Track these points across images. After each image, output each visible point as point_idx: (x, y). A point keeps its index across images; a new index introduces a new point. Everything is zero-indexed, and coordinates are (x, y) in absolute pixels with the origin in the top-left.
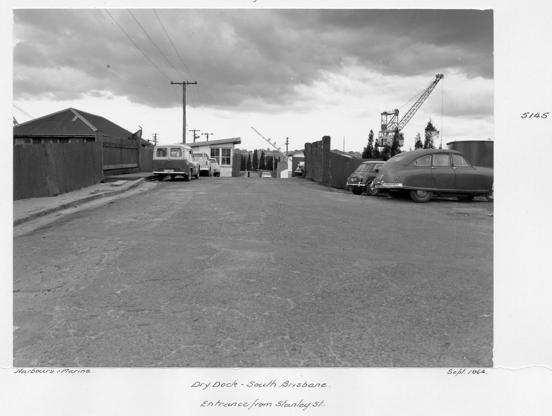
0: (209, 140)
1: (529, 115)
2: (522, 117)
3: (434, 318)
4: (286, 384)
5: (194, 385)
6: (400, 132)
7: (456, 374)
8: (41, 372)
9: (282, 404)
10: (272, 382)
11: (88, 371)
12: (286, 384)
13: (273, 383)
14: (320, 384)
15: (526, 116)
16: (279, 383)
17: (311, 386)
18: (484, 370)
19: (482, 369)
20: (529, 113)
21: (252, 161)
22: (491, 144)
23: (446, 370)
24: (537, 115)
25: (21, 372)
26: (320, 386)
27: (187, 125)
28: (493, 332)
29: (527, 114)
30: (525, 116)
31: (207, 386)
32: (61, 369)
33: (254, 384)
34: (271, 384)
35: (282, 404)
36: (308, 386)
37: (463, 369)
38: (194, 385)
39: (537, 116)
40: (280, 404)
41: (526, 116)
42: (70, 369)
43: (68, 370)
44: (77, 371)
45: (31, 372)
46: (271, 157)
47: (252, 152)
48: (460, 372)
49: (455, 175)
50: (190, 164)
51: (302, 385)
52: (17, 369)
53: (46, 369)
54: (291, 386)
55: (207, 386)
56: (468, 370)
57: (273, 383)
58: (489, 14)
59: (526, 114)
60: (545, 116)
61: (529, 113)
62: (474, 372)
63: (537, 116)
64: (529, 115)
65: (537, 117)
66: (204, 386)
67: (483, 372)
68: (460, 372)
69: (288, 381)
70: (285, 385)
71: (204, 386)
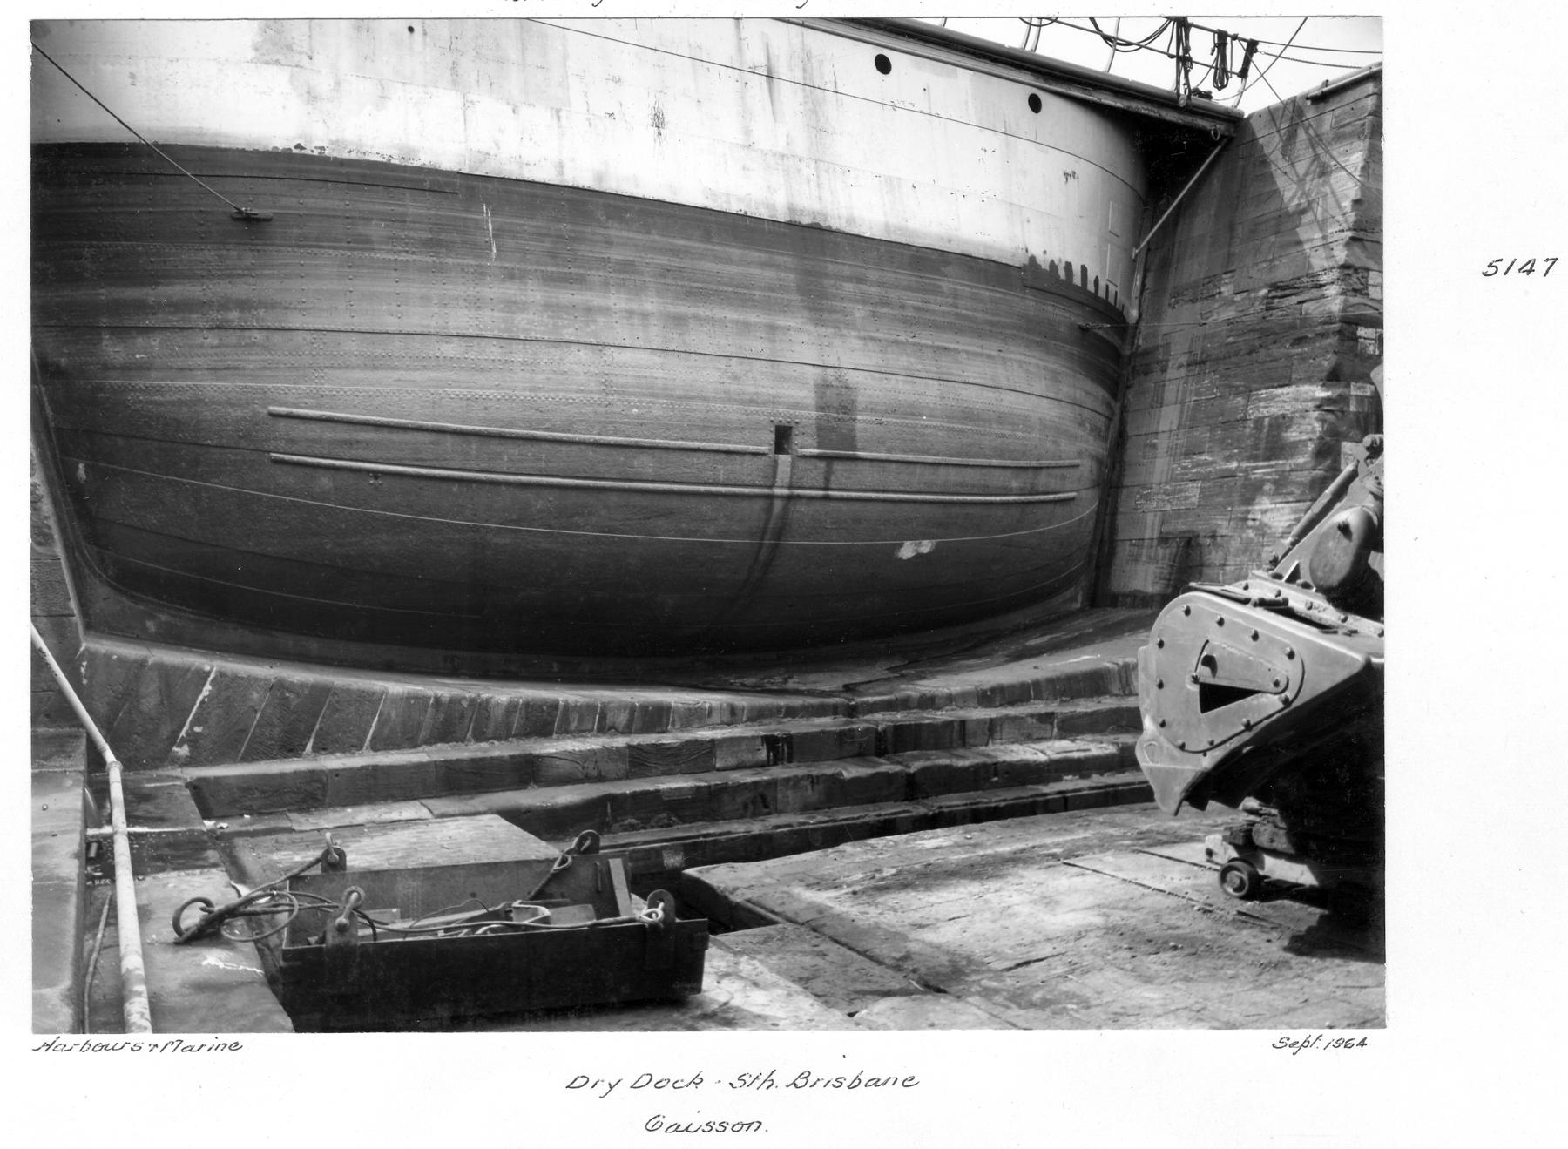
0: (946, 26)
1: (1502, 267)
2: (1484, 274)
4: (803, 1080)
5: (1551, 266)
7: (1295, 1050)
9: (749, 1081)
10: (763, 1078)
11: (236, 1046)
12: (803, 1080)
15: (1494, 269)
17: (876, 1082)
20: (1501, 260)
24: (1528, 268)
25: (53, 1047)
27: (883, 65)
30: (1492, 270)
31: (611, 1088)
34: (758, 1083)
35: (749, 1081)
37: (1315, 1033)
38: (1551, 266)
41: (1494, 269)
42: (191, 1039)
44: (156, 1046)
45: (80, 1047)
48: (1306, 1044)
49: (1202, 566)
50: (842, 324)
51: (846, 1084)
55: (611, 1088)
56: (1331, 1035)
61: (1501, 260)
62: (1284, 1043)
64: (1502, 267)
65: (1529, 272)
67: (1363, 1043)
68: (1306, 1044)
69: (760, 1123)
70: (800, 1082)
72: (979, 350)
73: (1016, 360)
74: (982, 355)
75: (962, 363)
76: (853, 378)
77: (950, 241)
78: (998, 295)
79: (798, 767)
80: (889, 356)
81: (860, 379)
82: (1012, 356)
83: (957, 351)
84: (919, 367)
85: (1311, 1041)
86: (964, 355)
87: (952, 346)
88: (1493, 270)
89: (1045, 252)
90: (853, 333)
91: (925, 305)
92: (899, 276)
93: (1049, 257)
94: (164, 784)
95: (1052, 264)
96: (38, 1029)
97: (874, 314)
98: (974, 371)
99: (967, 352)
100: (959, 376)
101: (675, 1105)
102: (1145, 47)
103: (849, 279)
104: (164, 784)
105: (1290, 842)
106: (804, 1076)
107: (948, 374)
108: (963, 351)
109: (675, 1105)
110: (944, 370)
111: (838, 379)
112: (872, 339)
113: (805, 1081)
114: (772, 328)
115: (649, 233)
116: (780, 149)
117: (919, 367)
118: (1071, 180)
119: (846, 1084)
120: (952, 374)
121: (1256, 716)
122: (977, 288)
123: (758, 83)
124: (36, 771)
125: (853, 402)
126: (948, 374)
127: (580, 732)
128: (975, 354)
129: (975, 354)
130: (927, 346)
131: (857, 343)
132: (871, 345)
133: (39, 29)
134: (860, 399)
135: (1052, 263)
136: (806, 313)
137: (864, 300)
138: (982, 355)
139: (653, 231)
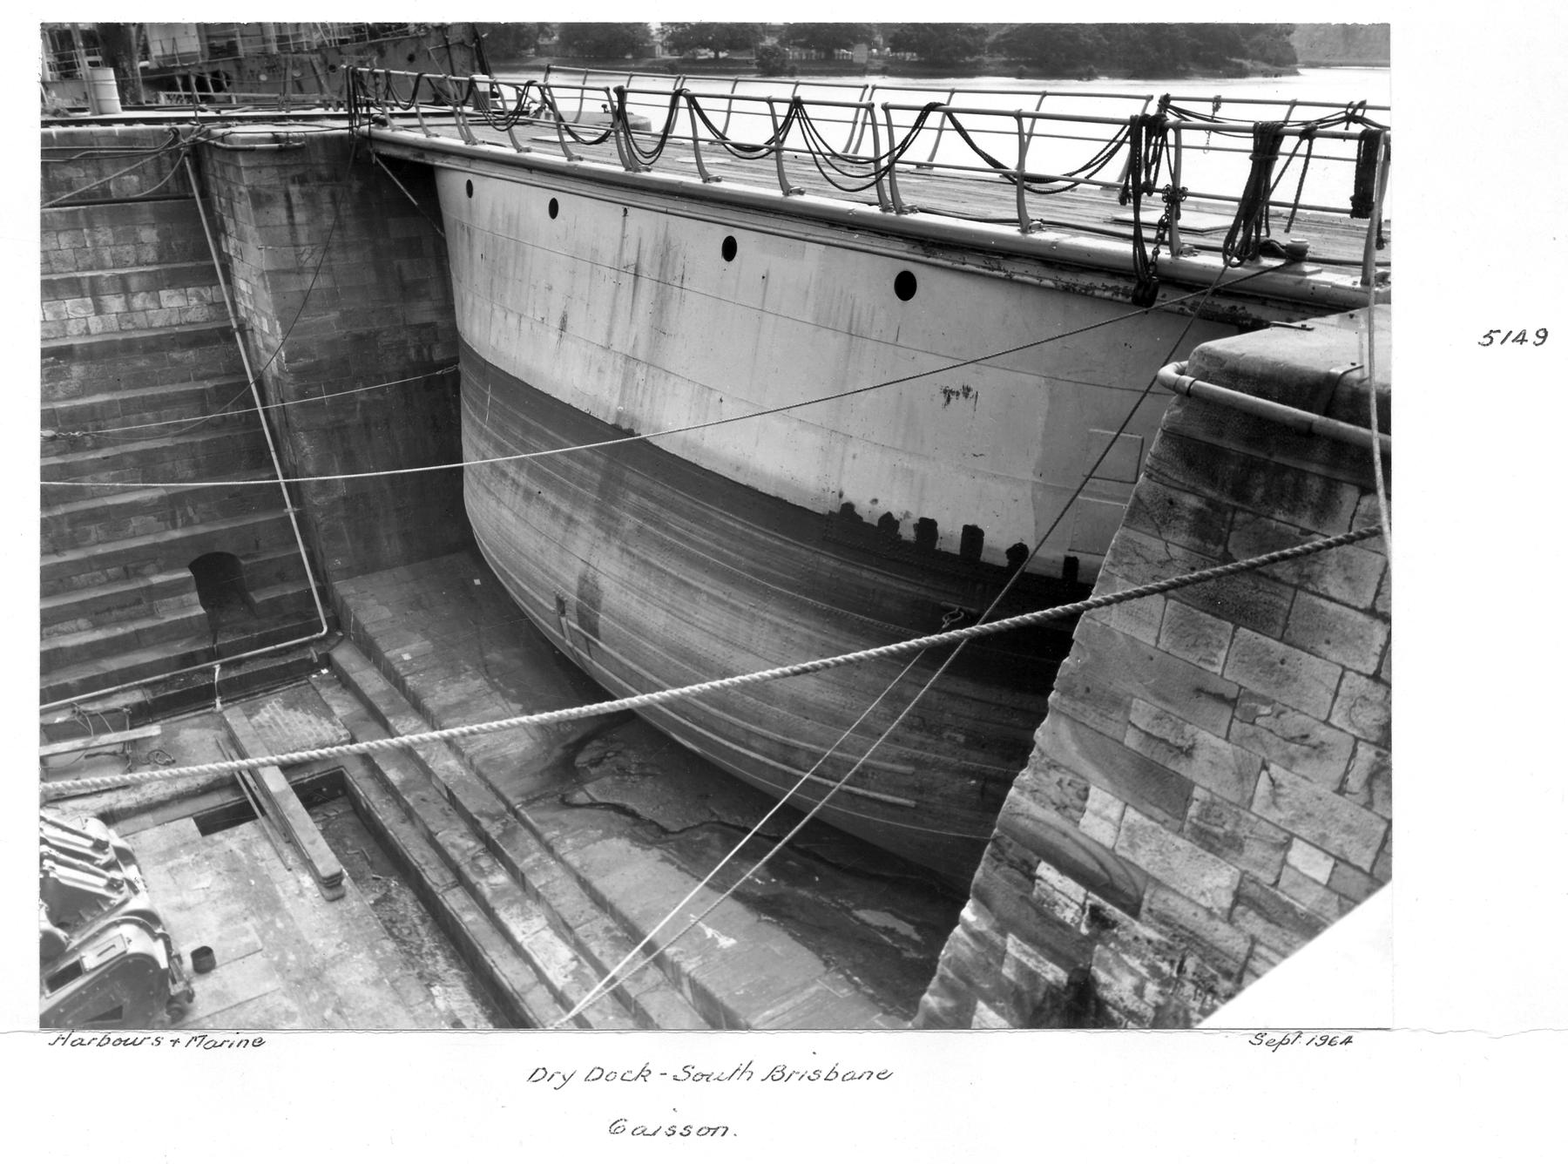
3: (1245, 951)
10: (742, 1069)
12: (778, 1074)
13: (744, 1071)
16: (761, 1070)
17: (850, 1077)
21: (826, 606)
22: (1389, 25)
26: (874, 1076)
28: (1390, 750)
29: (682, 1075)
30: (1488, 340)
33: (693, 1073)
34: (739, 1073)
36: (840, 1076)
43: (204, 1037)
45: (97, 1042)
51: (823, 1075)
52: (54, 1035)
57: (744, 1071)
58: (1385, 29)
63: (1521, 339)
64: (1498, 338)
71: (558, 1080)
72: (725, 597)
73: (770, 622)
74: (724, 603)
75: (698, 604)
76: (604, 582)
77: (738, 468)
78: (777, 543)
80: (635, 574)
81: (607, 585)
82: (768, 616)
83: (698, 590)
84: (655, 593)
86: (705, 597)
87: (695, 583)
89: (875, 501)
90: (618, 543)
91: (686, 533)
92: (676, 497)
93: (881, 509)
94: (707, 707)
95: (887, 519)
97: (640, 530)
98: (708, 615)
99: (709, 595)
100: (690, 615)
102: (1087, 180)
103: (635, 490)
104: (707, 707)
105: (154, 722)
107: (678, 610)
108: (705, 592)
110: (677, 605)
111: (594, 578)
112: (629, 553)
113: (780, 1074)
114: (570, 520)
116: (628, 352)
117: (655, 593)
118: (958, 403)
120: (683, 612)
121: (542, 955)
122: (750, 527)
123: (628, 279)
124: (51, 604)
125: (599, 601)
126: (678, 610)
128: (718, 600)
129: (718, 600)
130: (670, 575)
131: (616, 552)
132: (627, 559)
134: (603, 601)
135: (888, 516)
136: (594, 514)
137: (639, 512)
138: (724, 603)
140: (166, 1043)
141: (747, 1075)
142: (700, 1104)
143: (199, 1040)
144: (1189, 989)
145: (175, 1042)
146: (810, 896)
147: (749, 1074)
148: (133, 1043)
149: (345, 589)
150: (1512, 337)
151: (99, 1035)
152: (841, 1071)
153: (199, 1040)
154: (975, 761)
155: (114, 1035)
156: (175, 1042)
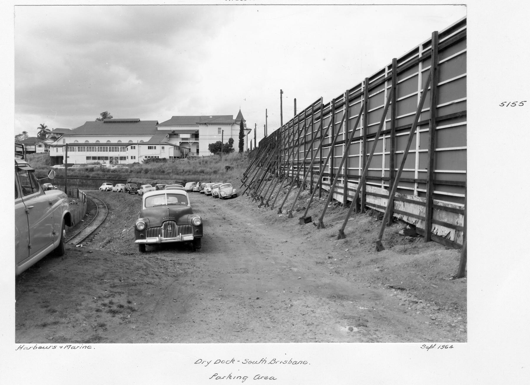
1: (506, 104)
2: (511, 106)
6: (224, 143)
8: (228, 362)
10: (263, 360)
11: (88, 347)
13: (263, 361)
14: (86, 347)
16: (268, 361)
17: (296, 363)
18: (452, 346)
19: (450, 344)
20: (506, 102)
23: (418, 345)
25: (23, 348)
30: (522, 104)
32: (64, 345)
34: (262, 362)
37: (434, 344)
39: (514, 104)
40: (245, 378)
42: (73, 345)
46: (234, 149)
47: (228, 143)
48: (432, 347)
51: (288, 362)
53: (48, 345)
54: (278, 363)
56: (438, 344)
57: (263, 361)
59: (503, 103)
60: (522, 104)
61: (506, 102)
64: (506, 104)
66: (206, 364)
67: (452, 347)
69: (504, 105)
71: (206, 364)
79: (405, 251)
85: (433, 346)
88: (503, 105)
96: (16, 342)
101: (223, 370)
106: (274, 360)
109: (223, 370)
115: (416, 133)
119: (288, 362)
127: (150, 244)
133: (233, 116)
139: (415, 132)
140: (58, 348)
141: (265, 362)
142: (265, 370)
143: (69, 347)
144: (425, 306)
145: (61, 347)
146: (283, 266)
147: (265, 362)
148: (43, 348)
149: (117, 166)
150: (511, 104)
151: (33, 345)
152: (293, 361)
153: (69, 347)
154: (441, 202)
155: (39, 345)
156: (61, 347)
